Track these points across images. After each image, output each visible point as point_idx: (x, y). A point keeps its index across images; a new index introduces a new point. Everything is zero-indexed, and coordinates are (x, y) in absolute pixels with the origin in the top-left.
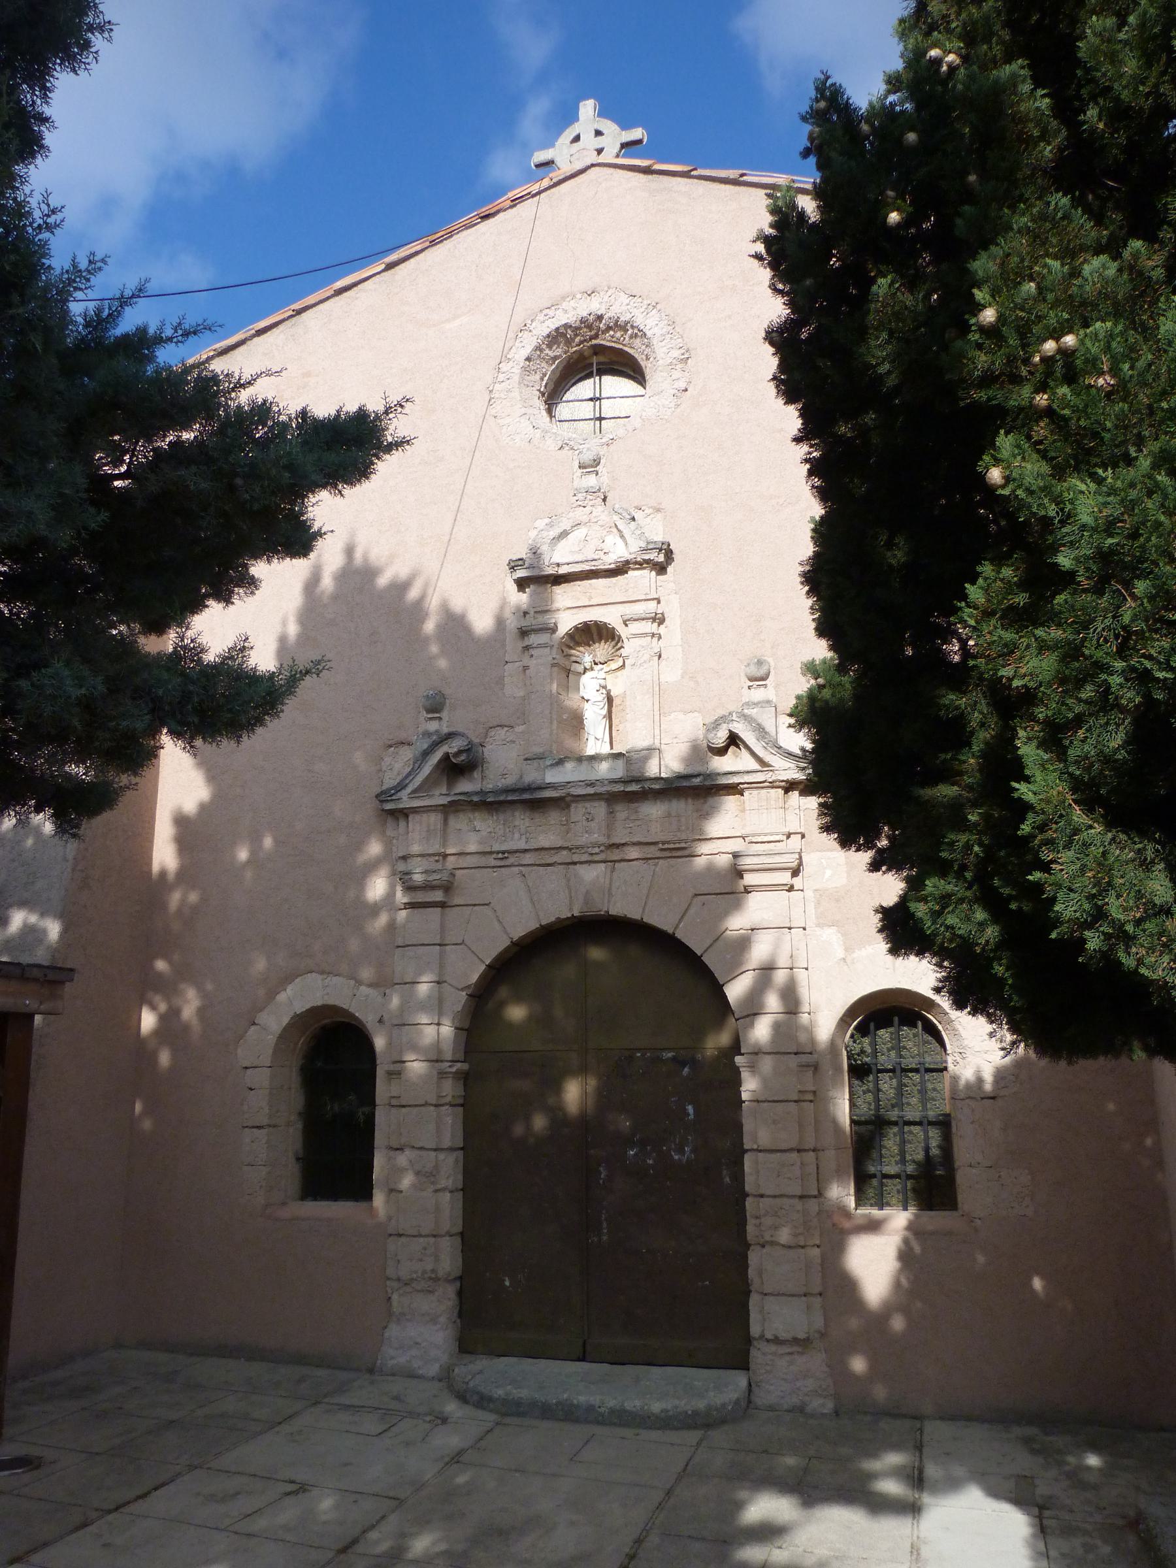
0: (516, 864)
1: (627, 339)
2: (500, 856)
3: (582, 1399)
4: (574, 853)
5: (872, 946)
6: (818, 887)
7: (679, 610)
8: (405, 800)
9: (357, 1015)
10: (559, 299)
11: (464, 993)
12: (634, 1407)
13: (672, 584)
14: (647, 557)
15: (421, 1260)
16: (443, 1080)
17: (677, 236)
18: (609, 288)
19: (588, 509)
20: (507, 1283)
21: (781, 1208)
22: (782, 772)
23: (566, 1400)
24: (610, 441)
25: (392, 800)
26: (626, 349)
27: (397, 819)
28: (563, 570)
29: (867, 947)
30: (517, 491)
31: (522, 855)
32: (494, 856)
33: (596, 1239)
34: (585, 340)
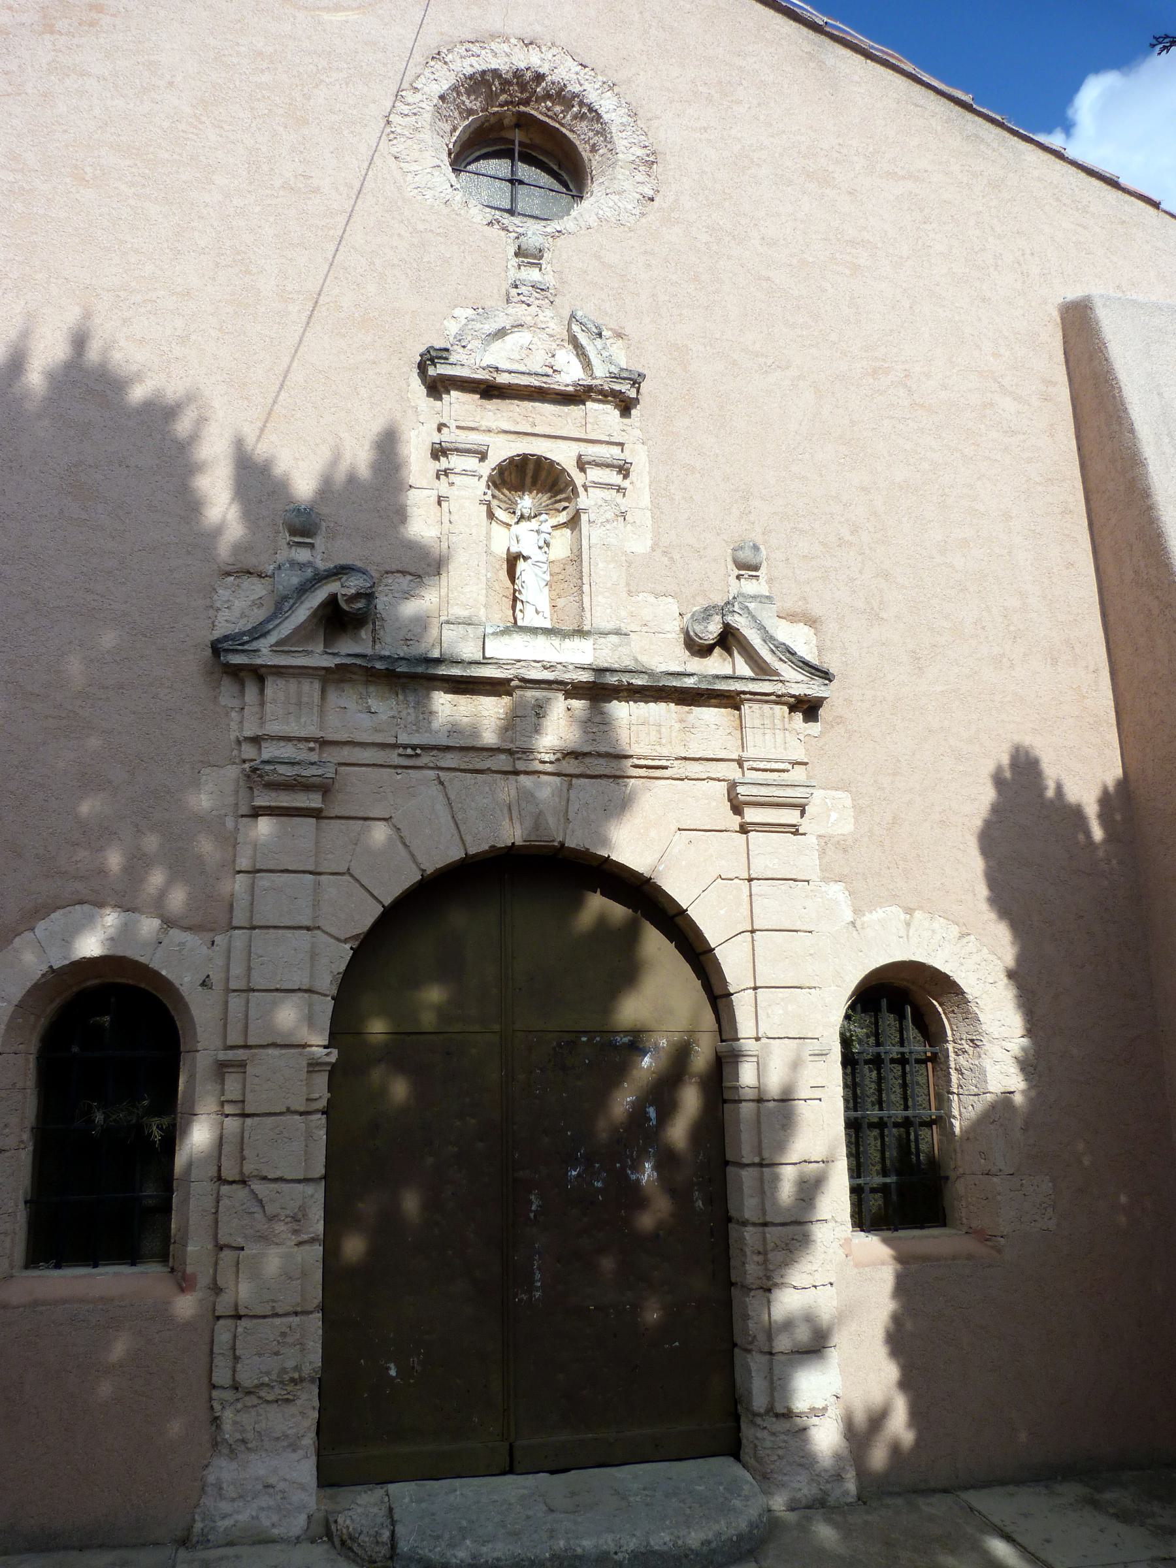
0: (431, 765)
1: (569, 117)
2: (409, 751)
3: (588, 1543)
4: (519, 759)
5: (884, 909)
6: (822, 832)
7: (647, 464)
8: (265, 654)
9: (164, 973)
10: (487, 35)
11: (348, 946)
12: (665, 1544)
13: (638, 431)
14: (617, 387)
15: (277, 1354)
16: (315, 1075)
17: (641, 13)
18: (553, 44)
19: (533, 309)
20: (393, 1373)
21: (793, 1239)
22: (793, 685)
23: (566, 1550)
24: (557, 234)
25: (243, 651)
26: (564, 130)
27: (242, 684)
28: (503, 379)
29: (878, 909)
30: (429, 262)
31: (441, 754)
32: (401, 751)
33: (525, 1297)
34: (512, 102)
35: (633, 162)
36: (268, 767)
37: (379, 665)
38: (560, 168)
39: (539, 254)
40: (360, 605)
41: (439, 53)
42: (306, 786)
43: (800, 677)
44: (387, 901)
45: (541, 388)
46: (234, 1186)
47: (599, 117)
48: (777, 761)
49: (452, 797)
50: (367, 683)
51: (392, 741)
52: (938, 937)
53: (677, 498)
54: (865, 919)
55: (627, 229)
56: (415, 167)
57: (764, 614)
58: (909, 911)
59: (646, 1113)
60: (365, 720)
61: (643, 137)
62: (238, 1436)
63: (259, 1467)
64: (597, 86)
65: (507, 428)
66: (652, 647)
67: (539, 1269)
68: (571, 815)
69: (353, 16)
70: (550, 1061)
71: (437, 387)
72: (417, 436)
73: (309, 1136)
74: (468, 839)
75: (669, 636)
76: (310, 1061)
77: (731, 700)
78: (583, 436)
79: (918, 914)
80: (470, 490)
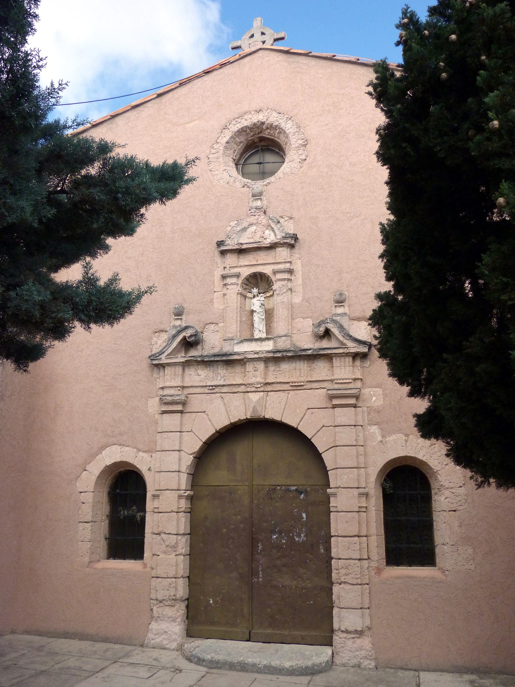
0: (219, 392)
2: (211, 388)
4: (248, 387)
8: (164, 360)
11: (192, 456)
14: (285, 241)
15: (168, 590)
16: (181, 500)
18: (268, 109)
19: (257, 217)
20: (211, 602)
22: (351, 349)
23: (242, 661)
25: (157, 359)
27: (159, 369)
28: (244, 247)
32: (208, 388)
33: (256, 580)
35: (298, 147)
36: (164, 398)
37: (199, 359)
38: (279, 151)
39: (261, 194)
40: (193, 339)
41: (226, 126)
42: (177, 403)
43: (354, 345)
44: (300, 428)
45: (258, 247)
46: (157, 535)
47: (285, 132)
48: (346, 379)
49: (226, 402)
50: (198, 365)
51: (205, 384)
52: (420, 445)
53: (312, 278)
54: (387, 439)
55: (294, 175)
56: (217, 172)
57: (343, 321)
58: (407, 435)
59: (302, 516)
60: (197, 378)
61: (303, 135)
62: (158, 615)
63: (164, 626)
64: (284, 120)
65: (247, 264)
66: (302, 339)
67: (261, 570)
68: (267, 406)
69: (196, 122)
70: (266, 496)
71: (223, 253)
72: (217, 273)
73: (178, 520)
74: (231, 417)
75: (308, 333)
76: (336, 496)
77: (329, 357)
78: (274, 262)
79: (411, 437)
80: (234, 290)
